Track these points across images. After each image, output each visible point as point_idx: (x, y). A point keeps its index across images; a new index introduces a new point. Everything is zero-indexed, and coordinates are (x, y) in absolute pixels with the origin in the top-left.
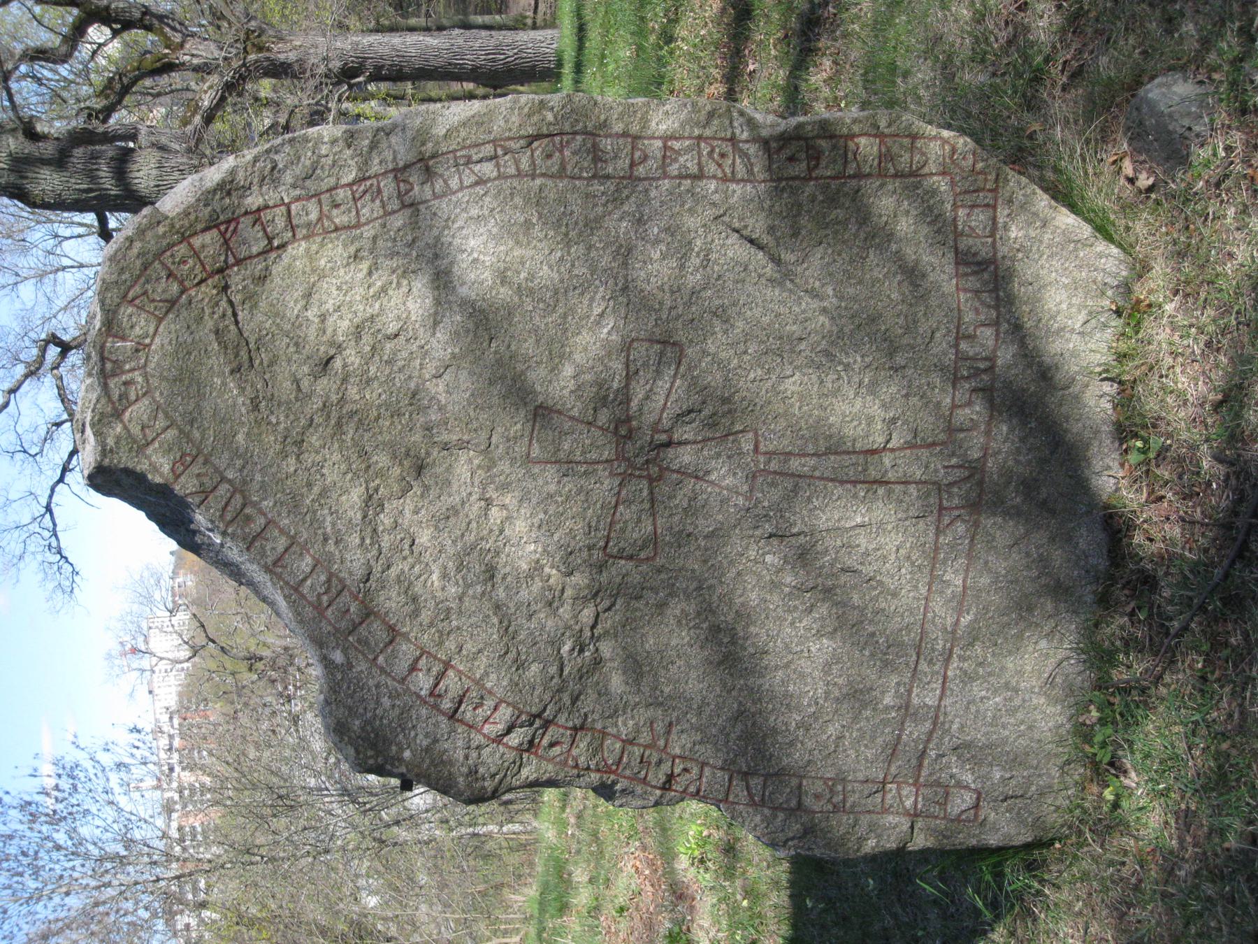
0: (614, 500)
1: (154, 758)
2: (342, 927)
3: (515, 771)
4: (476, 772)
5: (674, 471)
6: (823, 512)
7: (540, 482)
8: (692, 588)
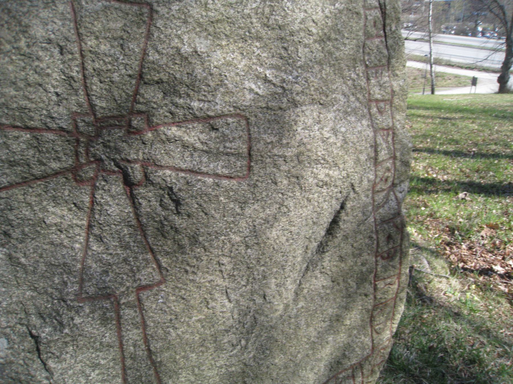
5: (93, 196)
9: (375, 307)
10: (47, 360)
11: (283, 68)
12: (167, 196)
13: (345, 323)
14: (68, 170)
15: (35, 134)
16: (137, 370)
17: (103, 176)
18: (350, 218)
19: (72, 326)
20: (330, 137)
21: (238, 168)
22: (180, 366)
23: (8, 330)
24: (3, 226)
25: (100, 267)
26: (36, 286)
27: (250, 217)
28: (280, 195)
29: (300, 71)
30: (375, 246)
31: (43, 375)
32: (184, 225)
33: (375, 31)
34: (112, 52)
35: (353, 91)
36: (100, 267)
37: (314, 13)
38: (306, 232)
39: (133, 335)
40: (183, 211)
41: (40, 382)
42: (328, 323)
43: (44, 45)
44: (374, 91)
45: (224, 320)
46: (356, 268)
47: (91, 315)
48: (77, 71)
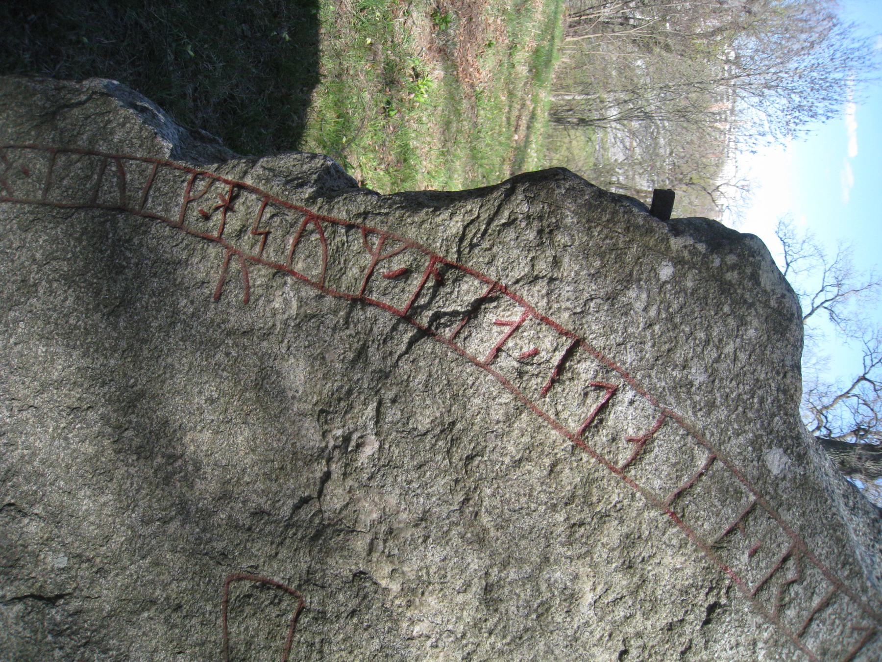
1: (746, 138)
2: (657, 50)
3: (473, 230)
4: (540, 232)
10: (24, 603)
19: (54, 645)
23: (73, 573)
26: (113, 618)
41: (2, 588)
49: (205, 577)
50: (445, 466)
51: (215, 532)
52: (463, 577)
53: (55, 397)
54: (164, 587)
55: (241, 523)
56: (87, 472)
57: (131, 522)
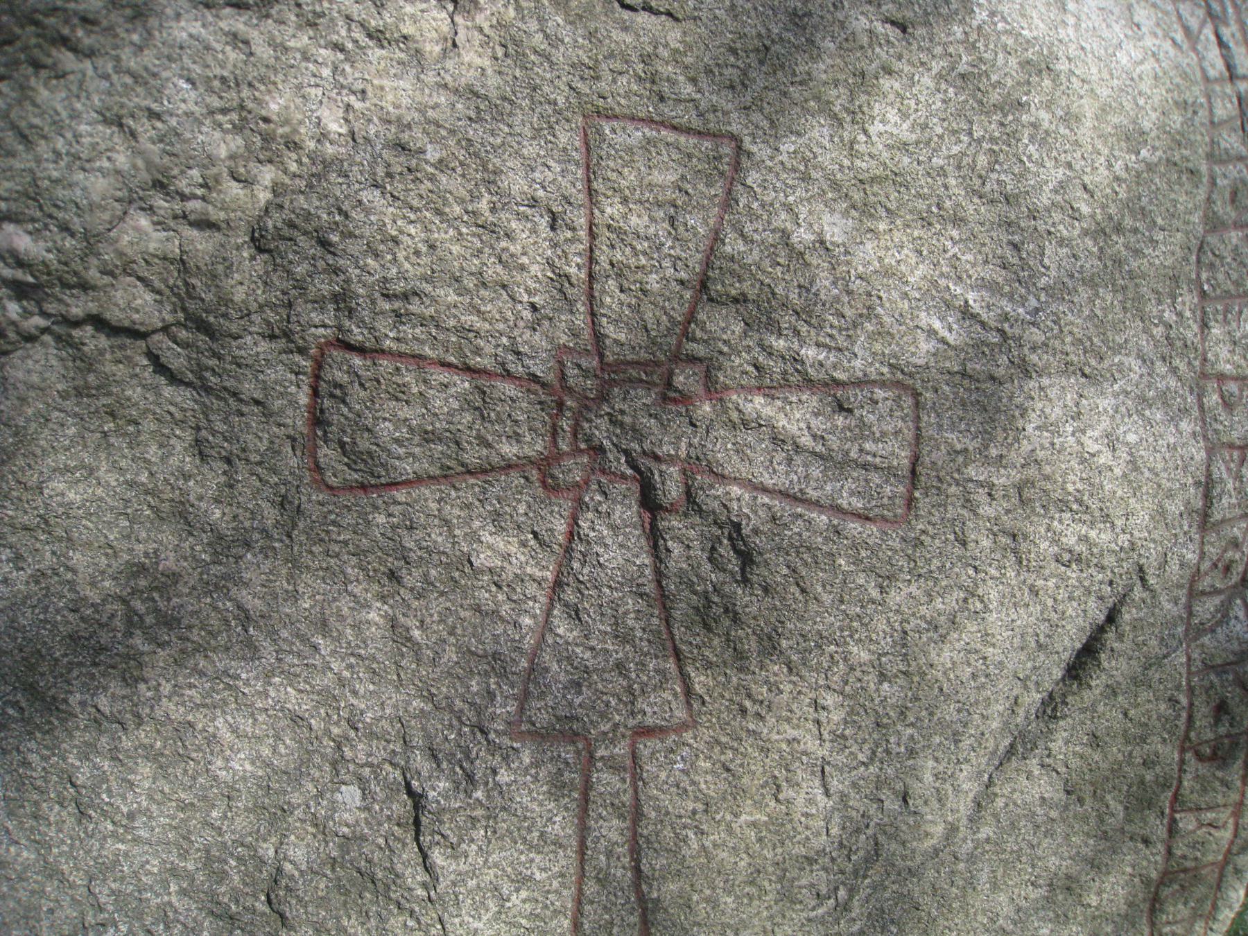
0: (485, 362)
5: (574, 521)
6: (497, 917)
7: (530, 150)
8: (245, 596)
9: (1167, 877)
10: (430, 848)
11: (1007, 289)
12: (725, 541)
13: (1086, 900)
14: (532, 463)
15: (480, 382)
16: (605, 907)
17: (599, 483)
18: (1126, 646)
19: (491, 785)
20: (1099, 452)
21: (885, 500)
22: (698, 919)
23: (366, 772)
24: (390, 559)
25: (566, 671)
26: (434, 690)
27: (897, 611)
28: (971, 572)
29: (1043, 299)
30: (1182, 723)
31: (419, 878)
32: (753, 609)
33: (1233, 214)
34: (652, 230)
35: (1166, 351)
36: (566, 671)
37: (1088, 170)
38: (1017, 663)
39: (611, 830)
40: (755, 579)
42: (1043, 892)
43: (522, 209)
44: (1217, 355)
45: (808, 833)
46: (1127, 769)
47: (533, 771)
48: (578, 265)
49: (328, 532)
50: (13, 89)
51: (247, 524)
52: (218, 47)
53: (66, 848)
54: (362, 606)
55: (222, 479)
56: (186, 771)
57: (257, 678)
